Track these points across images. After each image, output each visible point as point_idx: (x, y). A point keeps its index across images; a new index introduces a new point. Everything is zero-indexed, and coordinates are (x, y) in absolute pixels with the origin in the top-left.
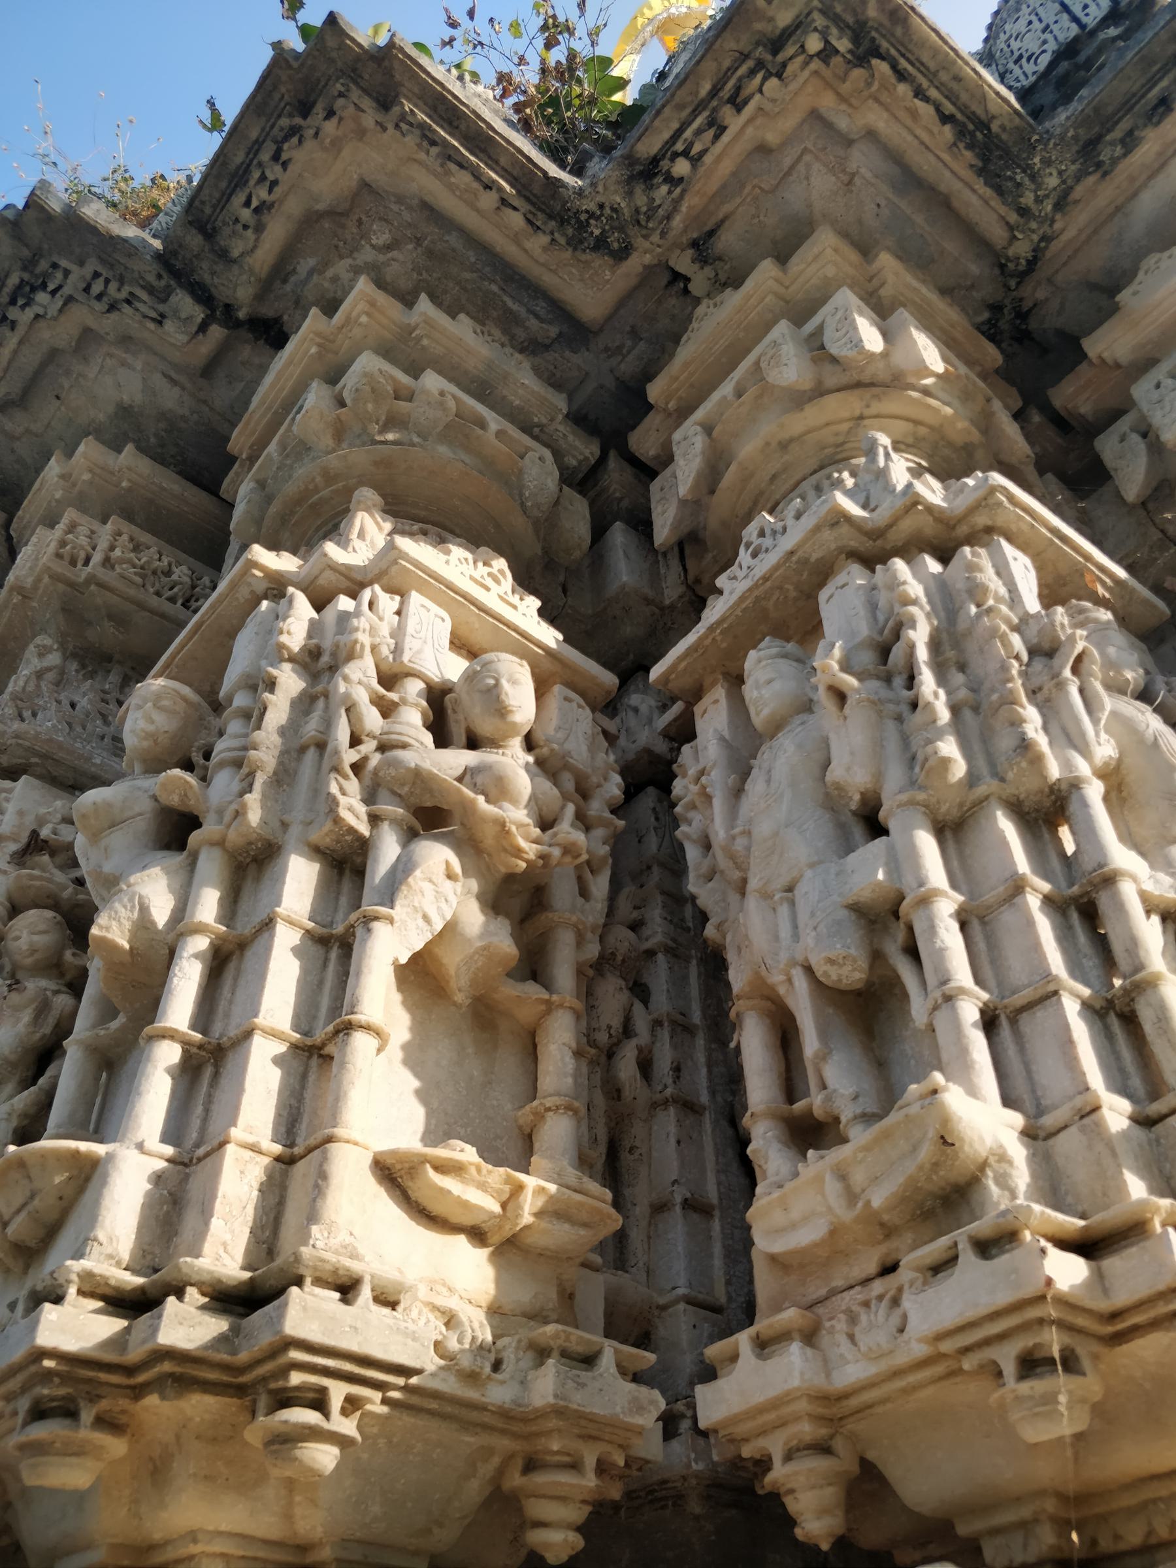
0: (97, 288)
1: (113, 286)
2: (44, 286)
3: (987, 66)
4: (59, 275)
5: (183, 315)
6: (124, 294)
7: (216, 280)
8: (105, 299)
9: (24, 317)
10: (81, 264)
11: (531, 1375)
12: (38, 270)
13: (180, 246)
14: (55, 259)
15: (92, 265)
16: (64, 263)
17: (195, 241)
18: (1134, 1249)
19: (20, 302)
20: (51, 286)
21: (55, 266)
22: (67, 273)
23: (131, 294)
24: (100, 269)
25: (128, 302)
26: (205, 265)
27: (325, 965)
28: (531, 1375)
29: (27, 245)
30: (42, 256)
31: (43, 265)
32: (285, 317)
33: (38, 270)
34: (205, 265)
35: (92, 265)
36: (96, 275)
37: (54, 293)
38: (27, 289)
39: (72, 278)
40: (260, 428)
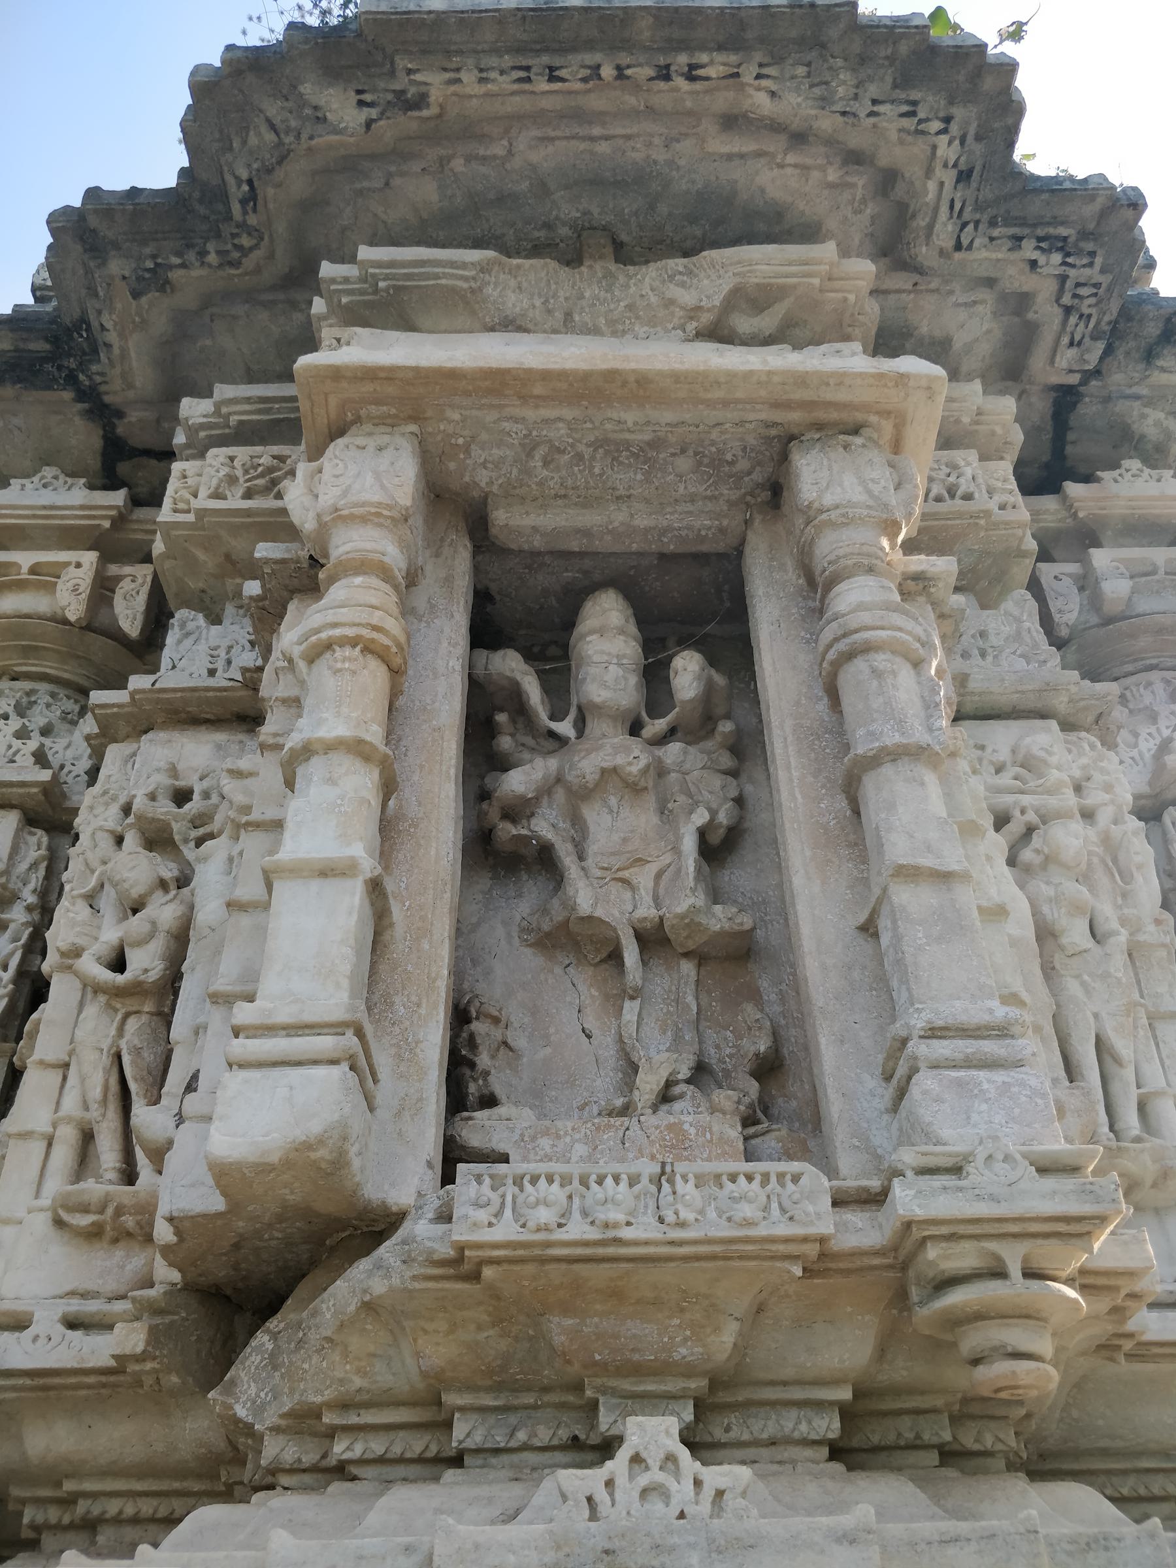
0: (1084, 291)
1: (1092, 300)
2: (1068, 255)
3: (894, 353)
4: (1085, 261)
5: (1086, 357)
6: (1086, 311)
7: (1121, 357)
8: (1076, 301)
9: (1028, 250)
10: (1103, 271)
11: (379, 870)
12: (1082, 244)
13: (1141, 321)
14: (1099, 252)
15: (1105, 280)
16: (1098, 261)
17: (1153, 330)
18: (457, 722)
19: (1042, 245)
20: (1070, 260)
21: (1092, 254)
22: (1091, 265)
23: (1090, 316)
24: (1104, 286)
25: (1081, 316)
26: (1132, 344)
27: (205, 416)
28: (379, 870)
29: (1098, 224)
30: (1095, 240)
31: (1089, 246)
32: (1087, 399)
33: (1082, 244)
34: (1132, 344)
35: (1105, 280)
36: (1097, 285)
37: (1064, 263)
38: (1060, 244)
39: (1088, 271)
40: (1157, 511)
